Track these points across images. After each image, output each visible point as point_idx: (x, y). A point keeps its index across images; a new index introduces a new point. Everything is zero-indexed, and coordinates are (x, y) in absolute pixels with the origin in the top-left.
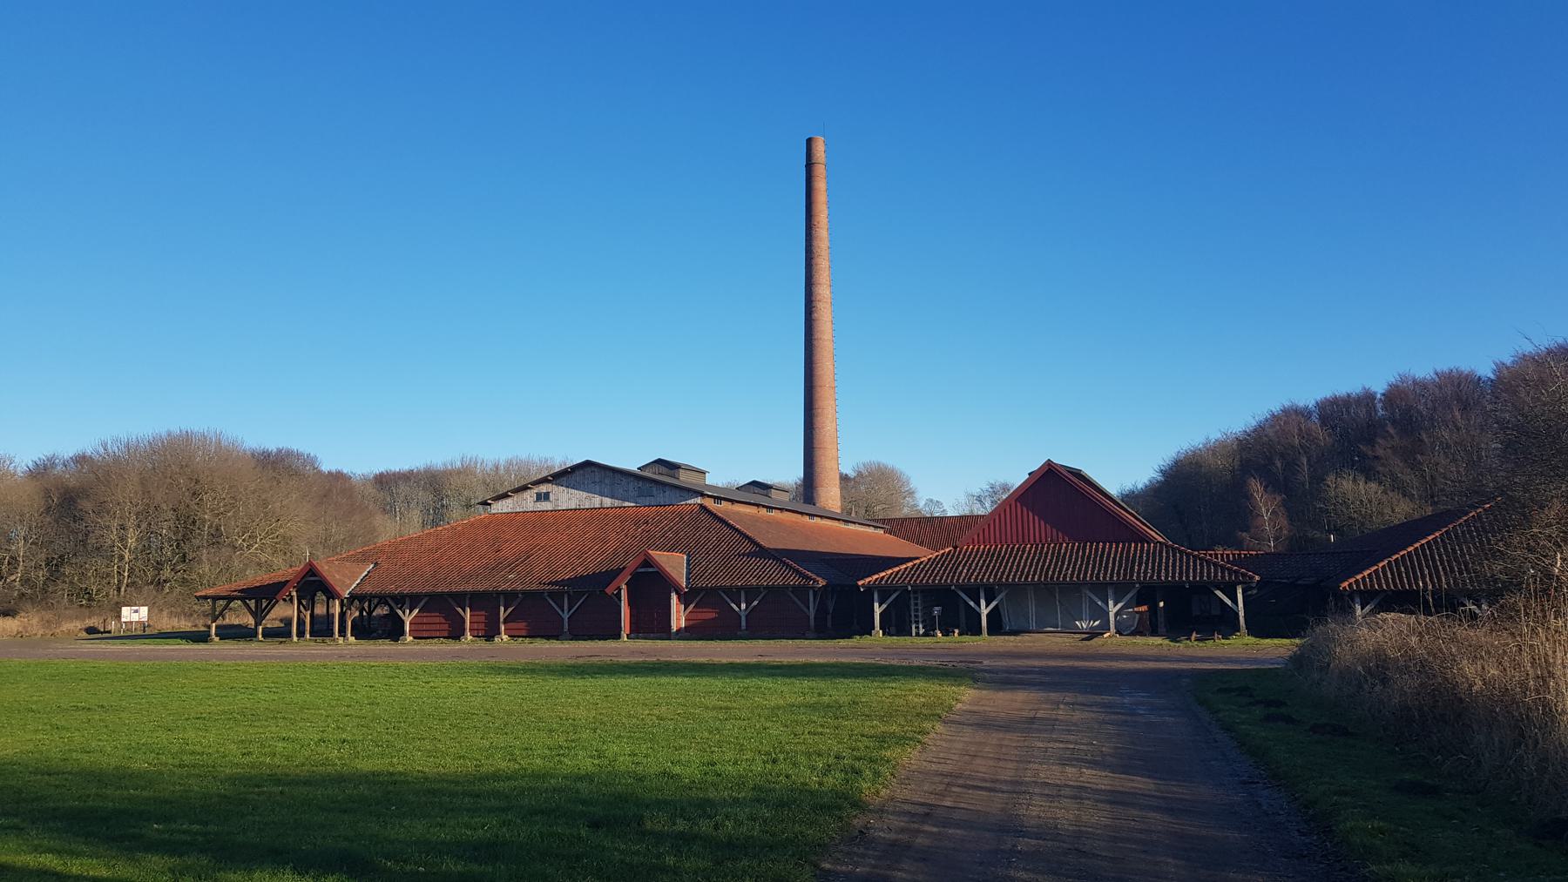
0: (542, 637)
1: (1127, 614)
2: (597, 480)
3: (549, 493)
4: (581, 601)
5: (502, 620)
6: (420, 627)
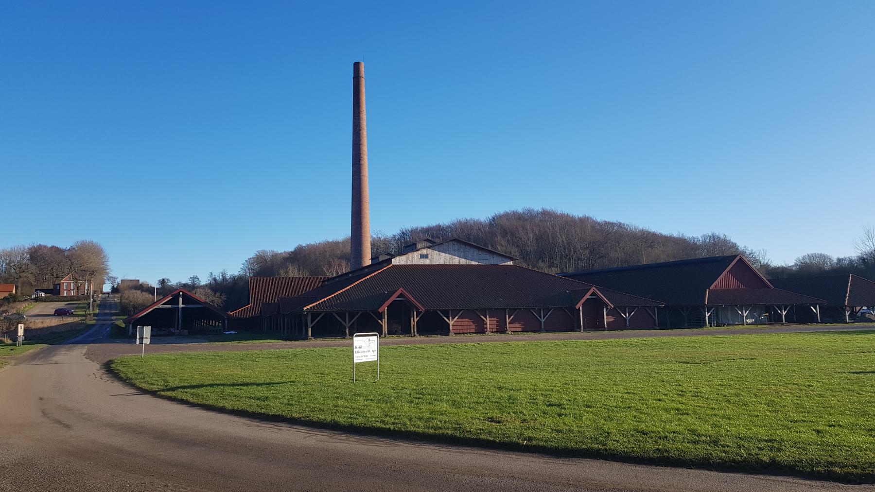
0: (532, 331)
1: (763, 316)
2: (456, 249)
3: (428, 254)
4: (569, 313)
5: (508, 323)
6: (458, 327)
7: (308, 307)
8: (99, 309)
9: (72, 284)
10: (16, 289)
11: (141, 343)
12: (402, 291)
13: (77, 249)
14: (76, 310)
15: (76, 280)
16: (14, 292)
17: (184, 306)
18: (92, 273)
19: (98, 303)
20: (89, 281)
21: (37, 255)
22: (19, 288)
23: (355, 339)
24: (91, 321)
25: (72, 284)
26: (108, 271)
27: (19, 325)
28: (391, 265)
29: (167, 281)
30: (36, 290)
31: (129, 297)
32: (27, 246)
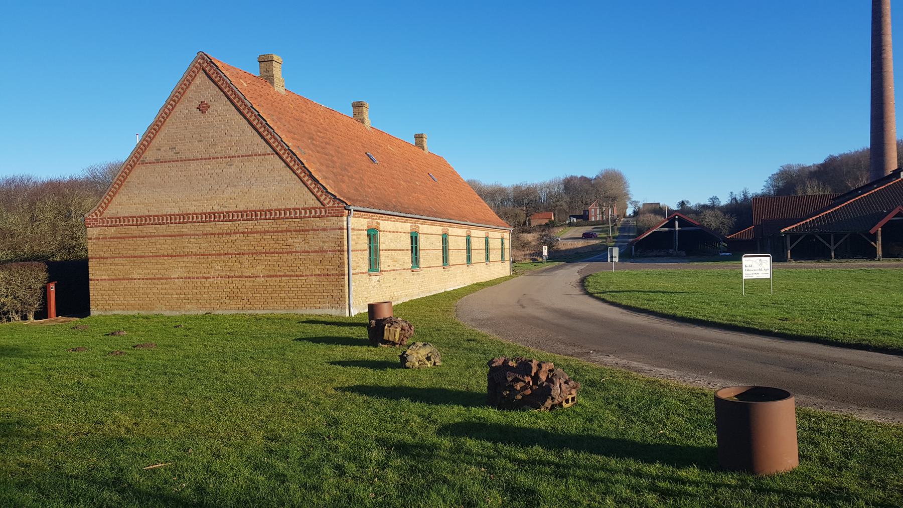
7: (787, 229)
8: (619, 232)
9: (598, 210)
10: (554, 216)
11: (612, 261)
12: (900, 209)
13: (601, 177)
14: (601, 234)
15: (601, 207)
16: (553, 218)
17: (680, 229)
18: (614, 199)
19: (619, 226)
20: (612, 207)
21: (570, 185)
22: (556, 215)
23: (744, 259)
24: (610, 243)
25: (598, 210)
26: (630, 196)
27: (544, 247)
28: (900, 179)
29: (686, 203)
30: (570, 216)
31: (643, 221)
32: (562, 177)
